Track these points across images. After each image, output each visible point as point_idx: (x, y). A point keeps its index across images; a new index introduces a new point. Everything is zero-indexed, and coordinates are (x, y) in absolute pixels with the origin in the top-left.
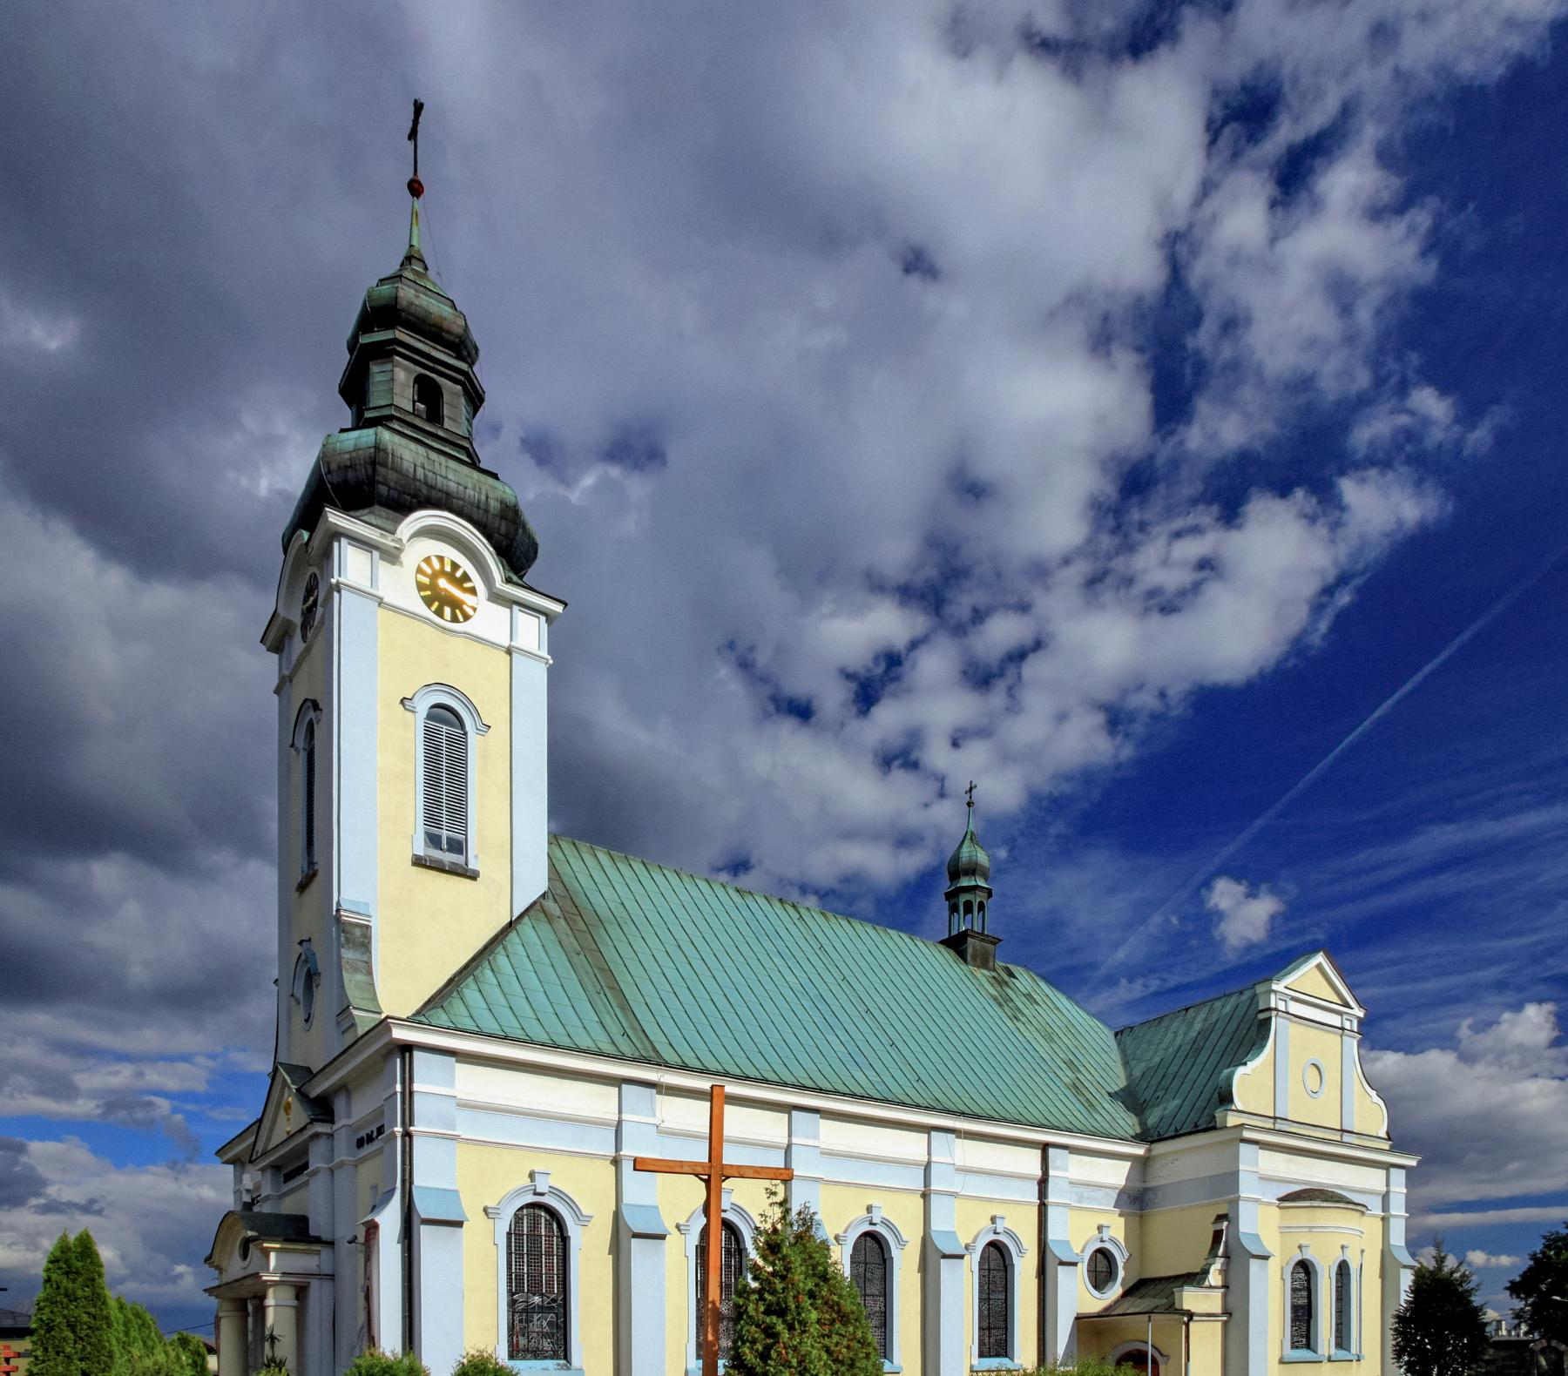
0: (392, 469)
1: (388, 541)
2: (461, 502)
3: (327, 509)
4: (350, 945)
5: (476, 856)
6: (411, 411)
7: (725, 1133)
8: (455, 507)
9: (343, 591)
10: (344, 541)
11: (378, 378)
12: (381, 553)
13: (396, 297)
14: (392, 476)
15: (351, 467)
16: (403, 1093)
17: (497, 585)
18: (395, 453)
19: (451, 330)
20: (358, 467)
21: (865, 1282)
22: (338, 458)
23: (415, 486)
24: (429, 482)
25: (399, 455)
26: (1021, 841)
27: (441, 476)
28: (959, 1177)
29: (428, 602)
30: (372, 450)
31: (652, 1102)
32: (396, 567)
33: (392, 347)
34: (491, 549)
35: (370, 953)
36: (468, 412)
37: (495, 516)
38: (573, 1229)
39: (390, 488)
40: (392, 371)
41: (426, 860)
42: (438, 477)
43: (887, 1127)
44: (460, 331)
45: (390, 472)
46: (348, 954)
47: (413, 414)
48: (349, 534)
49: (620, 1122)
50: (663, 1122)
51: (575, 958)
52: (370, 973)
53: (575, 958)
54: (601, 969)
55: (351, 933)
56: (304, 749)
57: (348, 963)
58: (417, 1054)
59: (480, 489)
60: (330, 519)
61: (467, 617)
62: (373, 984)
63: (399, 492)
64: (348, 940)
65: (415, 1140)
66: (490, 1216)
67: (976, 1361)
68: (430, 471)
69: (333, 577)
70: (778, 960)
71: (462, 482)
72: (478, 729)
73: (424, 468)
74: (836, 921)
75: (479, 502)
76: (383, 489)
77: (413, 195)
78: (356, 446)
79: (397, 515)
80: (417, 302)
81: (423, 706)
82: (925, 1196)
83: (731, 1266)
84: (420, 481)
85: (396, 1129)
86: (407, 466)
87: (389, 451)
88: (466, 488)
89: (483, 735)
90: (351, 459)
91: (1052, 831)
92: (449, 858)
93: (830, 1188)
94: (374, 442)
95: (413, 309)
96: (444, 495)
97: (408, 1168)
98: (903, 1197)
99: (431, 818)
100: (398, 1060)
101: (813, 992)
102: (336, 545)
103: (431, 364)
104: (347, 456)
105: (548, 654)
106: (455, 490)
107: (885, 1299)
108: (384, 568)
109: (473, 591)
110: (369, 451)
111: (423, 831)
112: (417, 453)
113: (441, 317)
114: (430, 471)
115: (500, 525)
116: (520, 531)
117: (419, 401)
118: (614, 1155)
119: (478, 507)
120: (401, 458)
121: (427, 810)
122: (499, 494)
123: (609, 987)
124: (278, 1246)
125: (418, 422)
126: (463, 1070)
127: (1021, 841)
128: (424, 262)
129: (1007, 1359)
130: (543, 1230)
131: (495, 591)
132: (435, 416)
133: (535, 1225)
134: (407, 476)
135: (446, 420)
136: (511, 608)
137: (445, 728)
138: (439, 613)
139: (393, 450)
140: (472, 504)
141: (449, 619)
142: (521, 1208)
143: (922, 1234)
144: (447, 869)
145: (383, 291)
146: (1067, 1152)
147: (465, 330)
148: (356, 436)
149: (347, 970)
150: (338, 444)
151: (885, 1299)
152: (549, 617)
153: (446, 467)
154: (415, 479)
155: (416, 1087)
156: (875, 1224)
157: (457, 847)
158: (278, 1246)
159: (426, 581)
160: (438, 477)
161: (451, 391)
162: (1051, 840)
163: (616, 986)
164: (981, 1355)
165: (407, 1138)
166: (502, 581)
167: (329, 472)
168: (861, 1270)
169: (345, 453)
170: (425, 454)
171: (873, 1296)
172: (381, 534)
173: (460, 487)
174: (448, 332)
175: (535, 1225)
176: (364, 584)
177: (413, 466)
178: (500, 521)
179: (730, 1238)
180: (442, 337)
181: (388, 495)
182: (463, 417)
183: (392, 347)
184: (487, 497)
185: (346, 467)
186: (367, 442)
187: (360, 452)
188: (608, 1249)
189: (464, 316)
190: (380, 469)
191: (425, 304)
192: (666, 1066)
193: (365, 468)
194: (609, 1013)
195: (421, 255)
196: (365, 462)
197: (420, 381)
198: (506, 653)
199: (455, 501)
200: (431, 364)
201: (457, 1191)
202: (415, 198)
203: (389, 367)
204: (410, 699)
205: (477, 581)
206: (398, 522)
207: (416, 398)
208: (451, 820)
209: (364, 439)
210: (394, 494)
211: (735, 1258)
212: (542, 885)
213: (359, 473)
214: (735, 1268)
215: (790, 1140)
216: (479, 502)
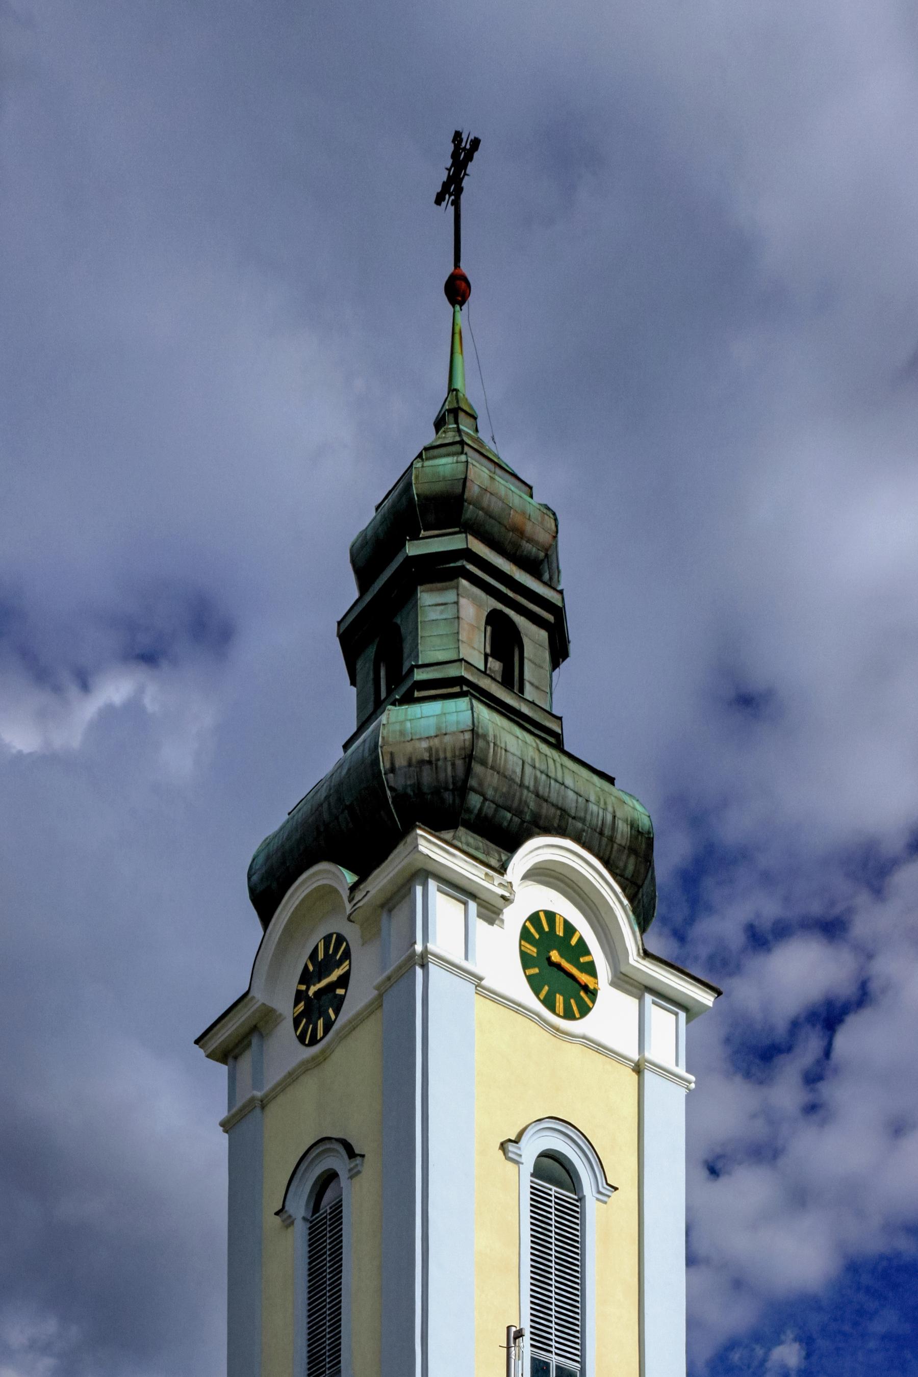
0: (492, 768)
1: (493, 886)
3: (419, 832)
6: (482, 668)
9: (432, 967)
11: (434, 615)
12: (479, 905)
14: (491, 780)
15: (430, 762)
17: (631, 961)
18: (498, 743)
19: (536, 538)
20: (440, 763)
22: (409, 747)
24: (541, 793)
25: (503, 745)
26: (823, 1344)
27: (556, 781)
30: (468, 736)
33: (459, 564)
34: (626, 902)
37: (622, 848)
39: (485, 799)
40: (457, 603)
45: (490, 771)
47: (484, 673)
56: (304, 1219)
60: (421, 848)
63: (498, 806)
72: (599, 1192)
73: (534, 767)
78: (439, 728)
81: (530, 1150)
84: (528, 788)
86: (513, 765)
87: (491, 738)
89: (605, 1203)
90: (430, 749)
91: (877, 1327)
94: (470, 723)
104: (424, 745)
105: (688, 1071)
108: (480, 927)
110: (461, 737)
111: (530, 1358)
114: (542, 772)
119: (601, 833)
125: (485, 683)
127: (823, 1344)
131: (624, 969)
134: (512, 780)
135: (528, 687)
136: (641, 999)
137: (554, 1190)
138: (549, 1003)
139: (495, 736)
141: (344, 990)
145: (441, 469)
148: (438, 712)
150: (408, 724)
153: (562, 765)
162: (872, 1344)
167: (393, 770)
169: (420, 739)
170: (534, 745)
172: (487, 874)
173: (580, 799)
176: (457, 956)
177: (520, 762)
178: (628, 857)
181: (481, 809)
183: (459, 564)
184: (614, 817)
185: (422, 762)
186: (458, 723)
187: (447, 739)
189: (554, 514)
190: (477, 768)
193: (453, 765)
195: (470, 406)
196: (454, 756)
197: (495, 619)
198: (633, 1070)
203: (450, 596)
207: (488, 651)
209: (453, 718)
210: (489, 809)
213: (442, 776)
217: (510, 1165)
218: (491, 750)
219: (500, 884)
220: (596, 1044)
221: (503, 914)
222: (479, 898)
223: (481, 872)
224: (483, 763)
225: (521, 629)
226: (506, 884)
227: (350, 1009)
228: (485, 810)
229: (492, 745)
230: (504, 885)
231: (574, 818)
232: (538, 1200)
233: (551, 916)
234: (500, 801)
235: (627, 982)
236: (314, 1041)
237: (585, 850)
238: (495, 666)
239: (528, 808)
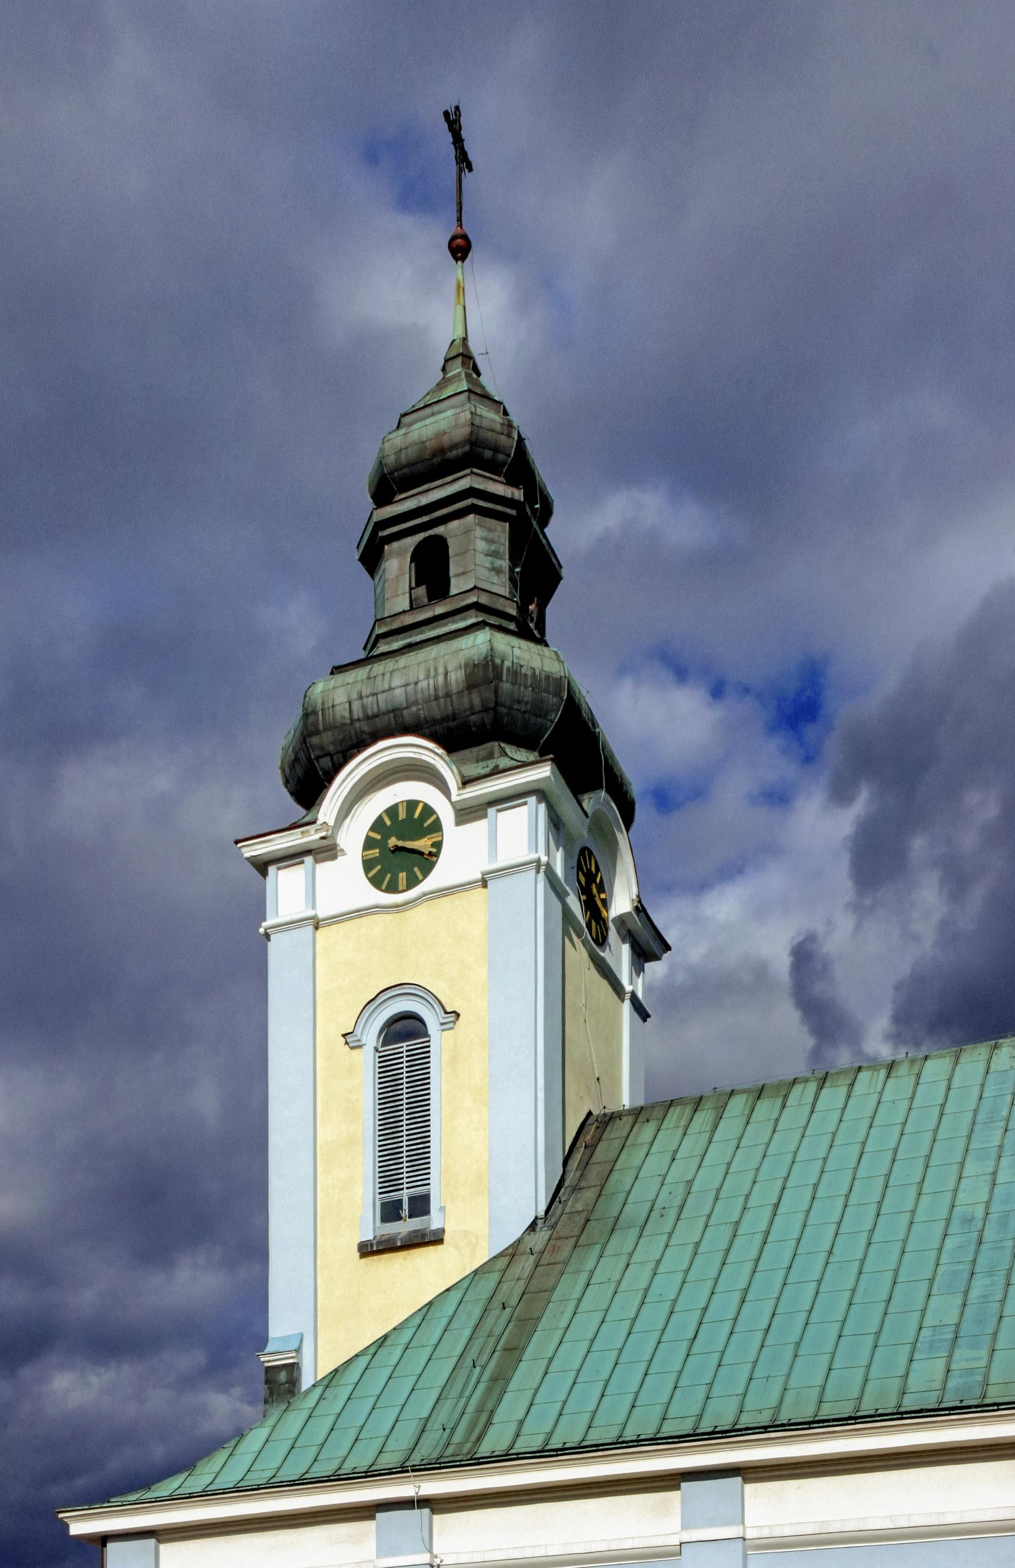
2: (414, 709)
37: (460, 693)
39: (331, 755)
43: (855, 1473)
72: (442, 1024)
81: (371, 1037)
89: (452, 1028)
99: (388, 1180)
103: (425, 519)
106: (403, 698)
108: (324, 869)
115: (471, 701)
126: (756, 1492)
140: (427, 701)
154: (352, 721)
157: (421, 1205)
172: (302, 832)
174: (454, 446)
180: (449, 460)
204: (352, 1033)
216: (436, 689)
219: (316, 831)
220: (439, 892)
221: (338, 845)
222: (314, 850)
223: (297, 835)
226: (321, 827)
227: (429, 884)
228: (337, 763)
229: (320, 713)
230: (319, 829)
231: (407, 708)
234: (339, 748)
235: (471, 813)
236: (392, 888)
237: (350, 762)
239: (365, 733)
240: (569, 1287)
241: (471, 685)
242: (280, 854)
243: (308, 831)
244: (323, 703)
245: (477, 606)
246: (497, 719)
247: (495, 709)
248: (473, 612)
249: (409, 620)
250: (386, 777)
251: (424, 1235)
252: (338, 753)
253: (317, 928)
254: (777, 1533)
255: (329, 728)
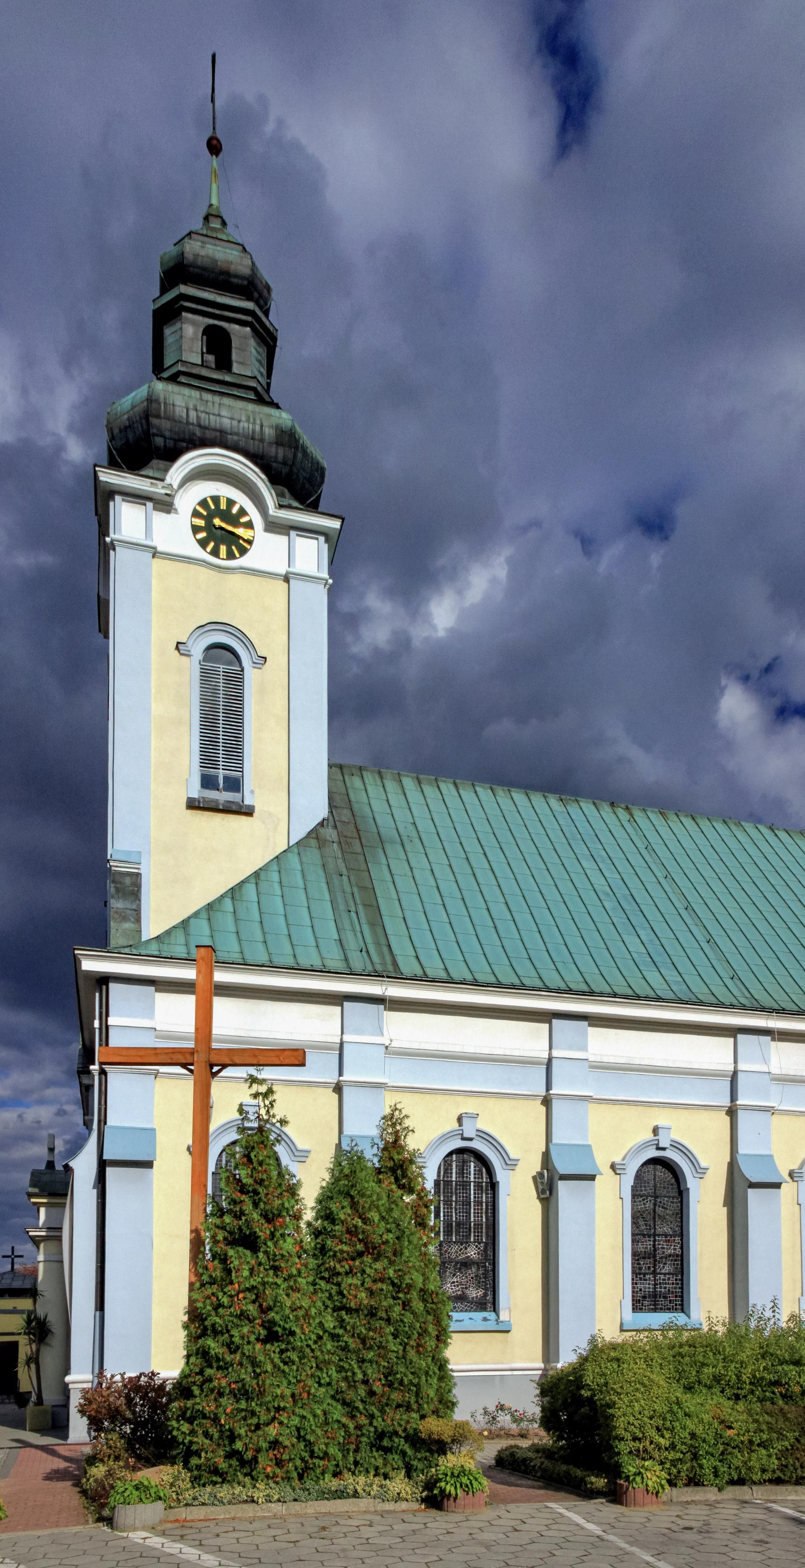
1: (158, 489)
4: (120, 894)
5: (252, 792)
7: (215, 1031)
8: (229, 443)
9: (117, 548)
10: (118, 498)
13: (183, 254)
14: (165, 425)
15: (130, 426)
16: (100, 1029)
21: (654, 1218)
23: (189, 430)
24: (202, 423)
25: (171, 402)
27: (214, 415)
28: (775, 1089)
29: (203, 544)
31: (380, 1019)
32: (172, 516)
34: (263, 476)
35: (140, 900)
36: (258, 352)
37: (270, 443)
38: (501, 1175)
39: (165, 438)
41: (199, 802)
42: (211, 416)
44: (246, 271)
46: (117, 904)
47: (202, 365)
48: (122, 489)
49: (342, 1044)
50: (391, 1041)
51: (336, 880)
52: (138, 920)
53: (336, 880)
54: (362, 888)
55: (120, 883)
57: (117, 912)
58: (112, 986)
59: (254, 419)
61: (243, 551)
62: (140, 931)
64: (118, 890)
65: (109, 1075)
66: (618, 1172)
67: (628, 1315)
68: (202, 412)
69: (108, 536)
70: (588, 864)
71: (236, 416)
72: (254, 663)
74: (677, 820)
75: (253, 431)
76: (159, 441)
77: (212, 153)
79: (167, 463)
80: (203, 253)
81: (198, 650)
82: (732, 1112)
83: (481, 1203)
84: (193, 424)
85: (92, 1067)
86: (180, 412)
87: (162, 400)
88: (239, 421)
89: (260, 668)
90: (128, 419)
92: (223, 797)
93: (604, 1107)
95: (199, 262)
96: (218, 434)
97: (103, 1107)
98: (704, 1117)
99: (208, 759)
100: (97, 995)
101: (621, 891)
102: (111, 504)
103: (218, 312)
104: (126, 417)
106: (229, 426)
107: (682, 1240)
108: (159, 518)
109: (249, 525)
112: (190, 397)
113: (228, 262)
114: (202, 412)
115: (277, 453)
116: (300, 455)
117: (208, 352)
118: (729, 1105)
119: (253, 438)
120: (173, 405)
121: (203, 751)
122: (274, 421)
123: (365, 905)
124: (45, 1201)
125: (205, 372)
128: (221, 217)
129: (682, 1315)
130: (454, 1175)
131: (270, 519)
132: (224, 363)
133: (462, 1171)
136: (289, 535)
138: (215, 553)
139: (165, 399)
140: (246, 437)
142: (450, 1154)
143: (728, 1159)
144: (221, 807)
146: (152, 989)
147: (252, 270)
149: (116, 919)
151: (682, 1240)
152: (324, 533)
153: (220, 404)
154: (188, 423)
155: (111, 1021)
156: (664, 1149)
157: (234, 785)
158: (45, 1201)
159: (201, 523)
160: (211, 416)
161: (240, 334)
163: (375, 904)
164: (637, 1307)
165: (103, 1077)
166: (276, 507)
168: (649, 1205)
171: (666, 1236)
172: (152, 483)
174: (237, 276)
175: (462, 1171)
179: (480, 1171)
181: (165, 446)
182: (254, 360)
185: (126, 428)
188: (722, 1199)
190: (154, 421)
191: (210, 253)
192: (388, 977)
194: (354, 930)
196: (140, 418)
197: (209, 331)
199: (229, 437)
200: (218, 312)
201: (154, 1130)
202: (214, 157)
205: (254, 514)
206: (167, 470)
207: (205, 350)
208: (227, 758)
211: (487, 1194)
212: (321, 811)
214: (487, 1206)
215: (550, 1054)
216: (253, 431)
217: (184, 658)
218: (162, 407)
219: (163, 487)
224: (158, 416)
225: (228, 330)
229: (163, 405)
232: (206, 676)
233: (216, 499)
234: (176, 437)
238: (211, 358)
240: (379, 873)
241: (278, 443)
242: (128, 490)
243: (156, 485)
244: (165, 399)
245: (254, 389)
246: (290, 474)
247: (291, 466)
248: (252, 393)
249: (195, 371)
250: (213, 474)
251: (241, 807)
252: (171, 439)
253: (153, 557)
254: (605, 1060)
255: (168, 418)
